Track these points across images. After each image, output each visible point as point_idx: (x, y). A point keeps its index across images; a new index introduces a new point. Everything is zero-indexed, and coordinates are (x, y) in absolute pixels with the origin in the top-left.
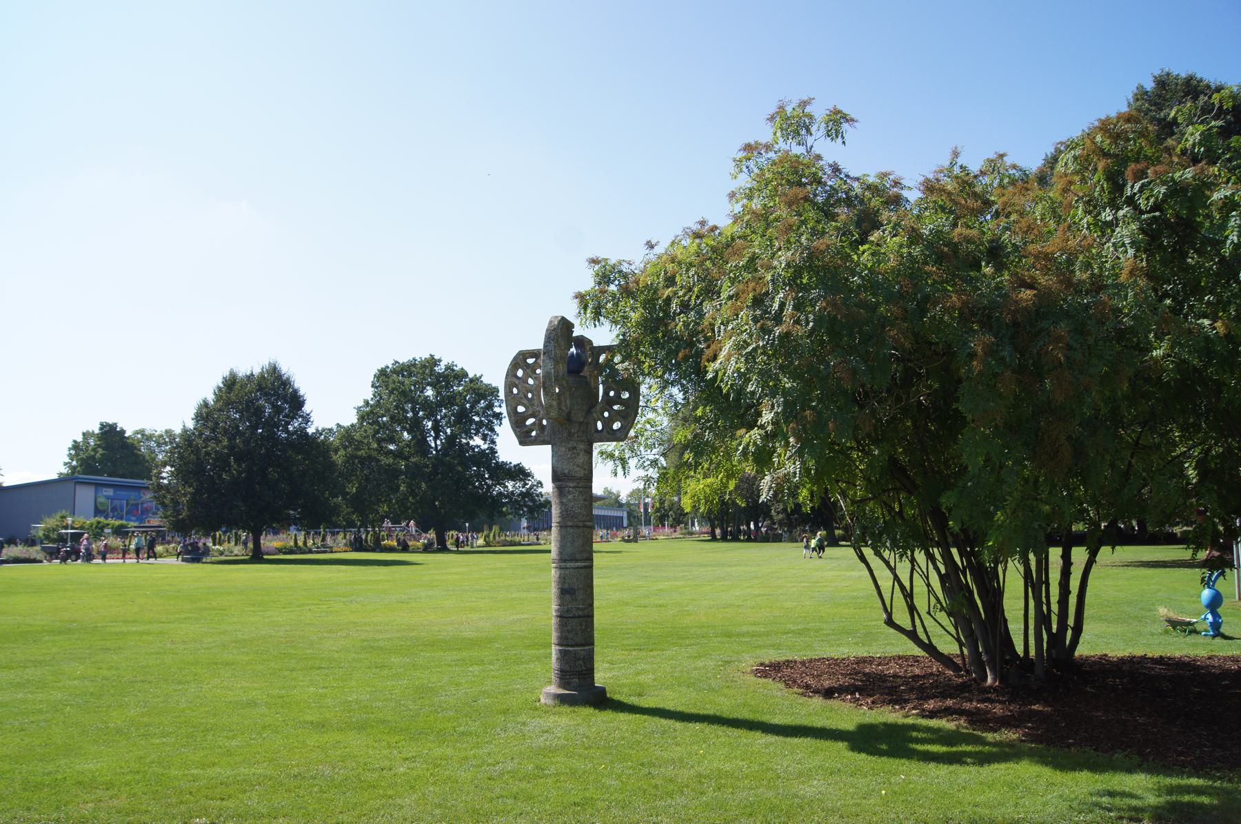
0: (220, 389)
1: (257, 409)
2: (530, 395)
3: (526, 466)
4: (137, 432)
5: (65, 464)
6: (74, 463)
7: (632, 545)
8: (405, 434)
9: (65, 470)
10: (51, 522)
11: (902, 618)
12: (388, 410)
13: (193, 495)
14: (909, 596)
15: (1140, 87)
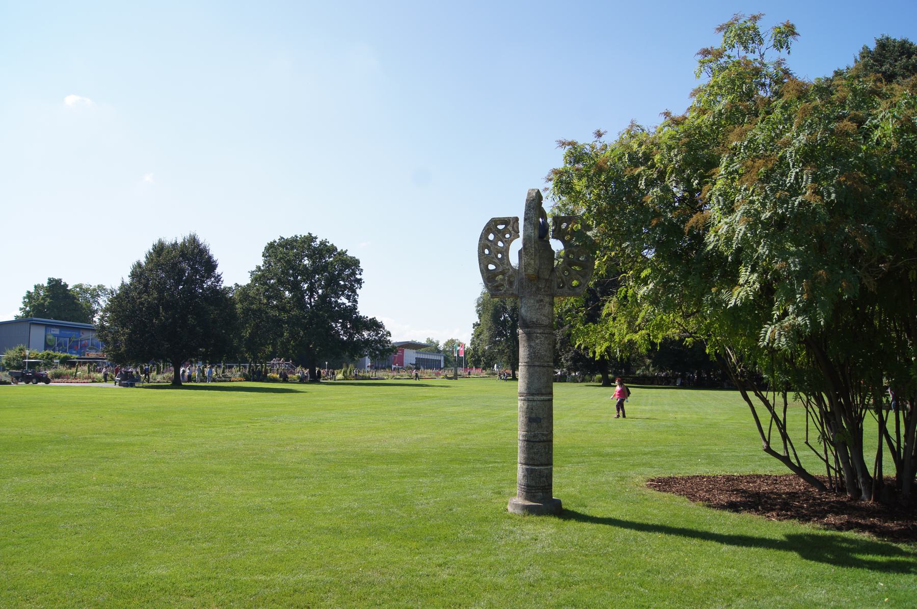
0: (150, 253)
1: (179, 269)
2: (500, 256)
3: (379, 320)
4: (76, 287)
5: (21, 309)
6: (28, 309)
7: (453, 381)
8: (287, 293)
9: (20, 314)
10: (12, 353)
11: (777, 444)
12: (276, 275)
13: (130, 335)
14: (782, 427)
15: (865, 48)
